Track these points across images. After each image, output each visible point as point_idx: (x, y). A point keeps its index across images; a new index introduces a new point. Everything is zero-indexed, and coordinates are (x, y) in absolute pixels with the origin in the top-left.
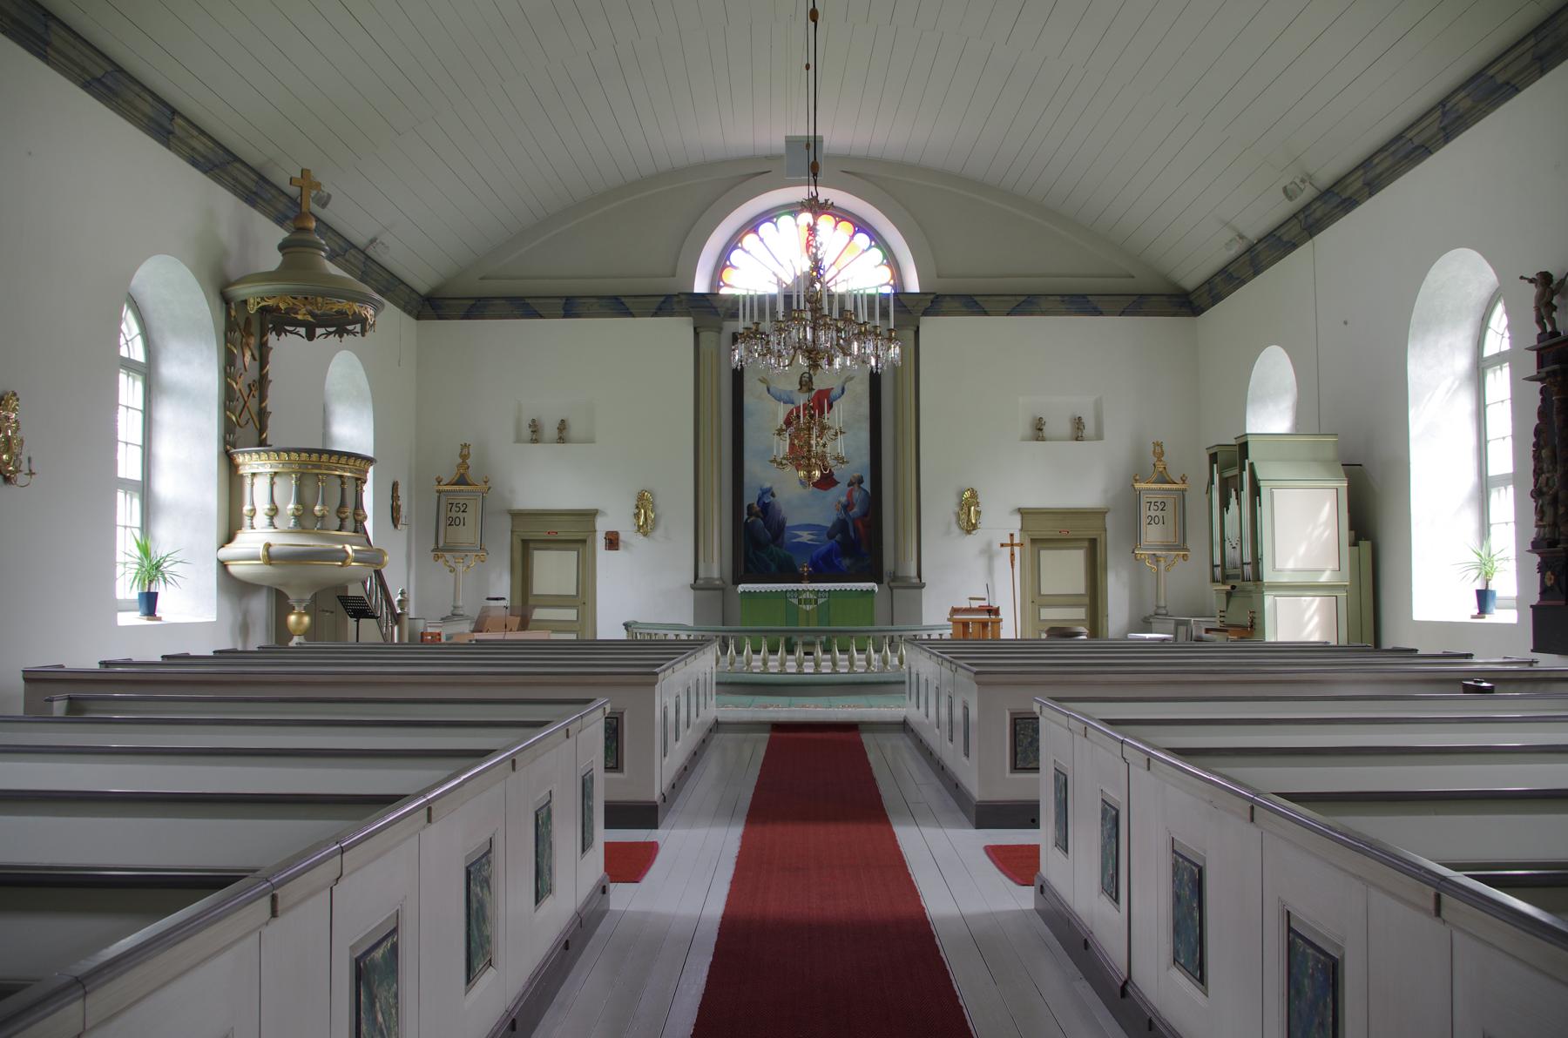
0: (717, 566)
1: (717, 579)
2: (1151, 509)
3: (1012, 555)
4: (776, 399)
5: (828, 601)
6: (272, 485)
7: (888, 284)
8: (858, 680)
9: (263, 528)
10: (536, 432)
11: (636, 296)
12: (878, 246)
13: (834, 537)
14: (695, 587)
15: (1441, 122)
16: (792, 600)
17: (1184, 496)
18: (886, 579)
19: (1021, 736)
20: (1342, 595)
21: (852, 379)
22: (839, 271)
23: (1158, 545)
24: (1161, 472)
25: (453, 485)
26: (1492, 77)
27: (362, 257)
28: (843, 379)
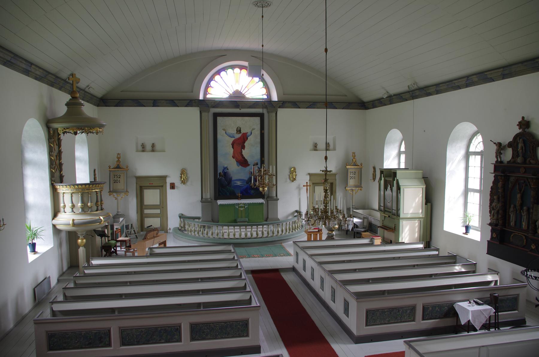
0: (209, 195)
1: (209, 199)
2: (351, 174)
3: (307, 189)
4: (228, 136)
5: (248, 207)
6: (72, 197)
7: (265, 94)
9: (69, 213)
10: (143, 148)
11: (179, 100)
13: (248, 183)
14: (202, 201)
15: (466, 82)
16: (236, 207)
17: (361, 170)
18: (266, 197)
19: (369, 316)
20: (422, 220)
21: (254, 129)
22: (248, 90)
23: (352, 186)
24: (355, 162)
25: (115, 168)
26: (486, 75)
27: (83, 92)
28: (251, 129)
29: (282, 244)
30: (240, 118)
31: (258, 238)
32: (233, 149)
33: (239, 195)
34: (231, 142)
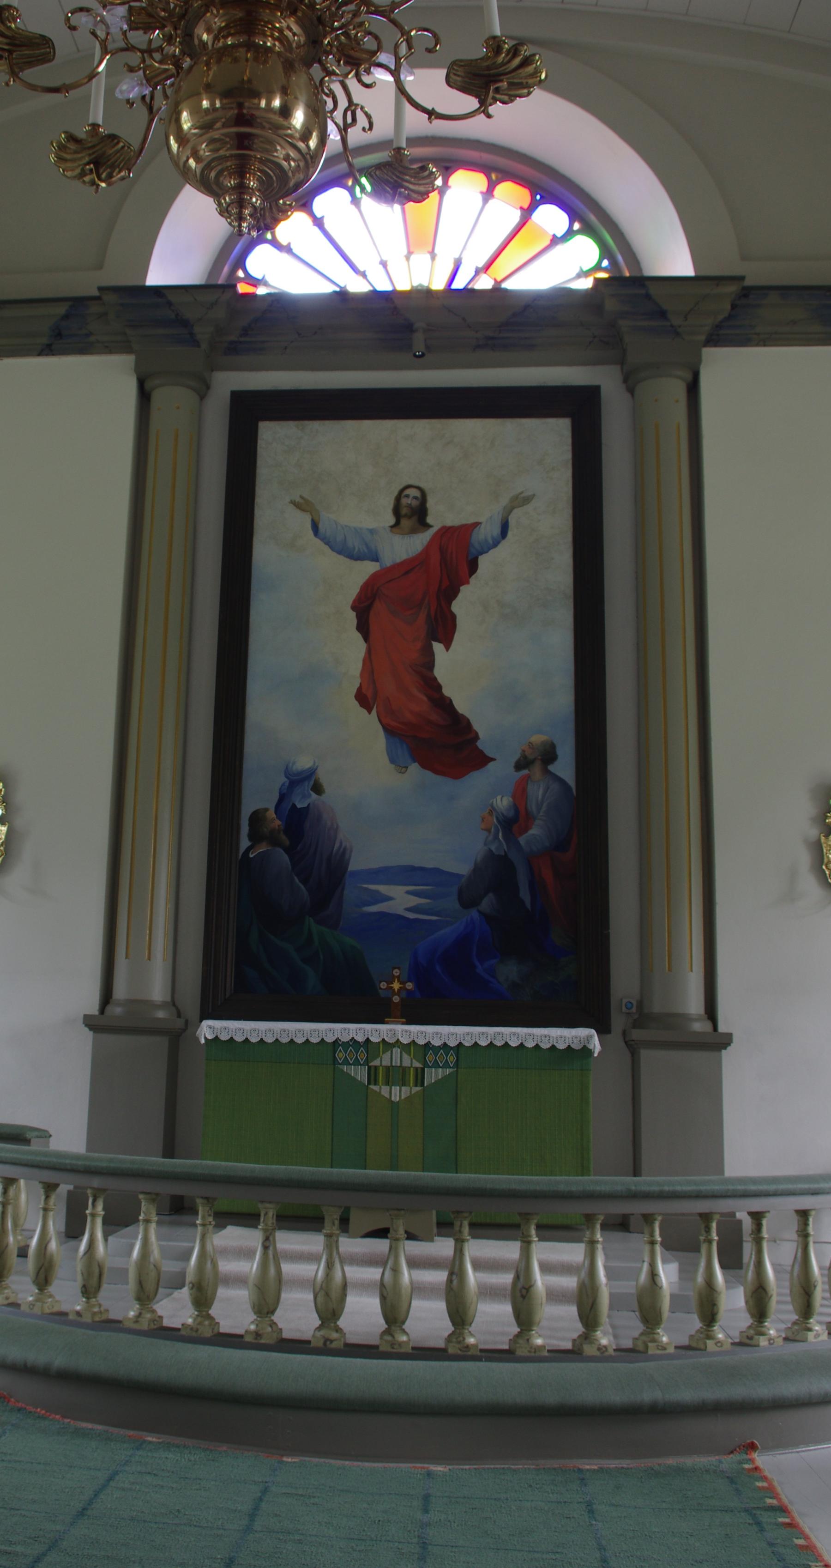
1: (163, 1006)
8: (550, 1397)
12: (588, 230)
16: (352, 1071)
18: (618, 1022)
28: (504, 501)
29: (761, 1459)
30: (421, 428)
31: (467, 1355)
32: (366, 638)
33: (396, 986)
34: (353, 592)
